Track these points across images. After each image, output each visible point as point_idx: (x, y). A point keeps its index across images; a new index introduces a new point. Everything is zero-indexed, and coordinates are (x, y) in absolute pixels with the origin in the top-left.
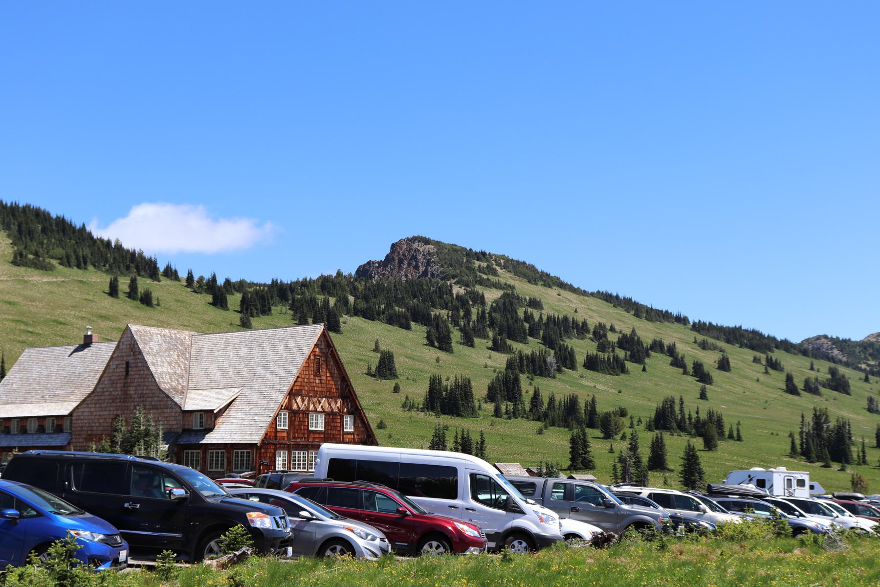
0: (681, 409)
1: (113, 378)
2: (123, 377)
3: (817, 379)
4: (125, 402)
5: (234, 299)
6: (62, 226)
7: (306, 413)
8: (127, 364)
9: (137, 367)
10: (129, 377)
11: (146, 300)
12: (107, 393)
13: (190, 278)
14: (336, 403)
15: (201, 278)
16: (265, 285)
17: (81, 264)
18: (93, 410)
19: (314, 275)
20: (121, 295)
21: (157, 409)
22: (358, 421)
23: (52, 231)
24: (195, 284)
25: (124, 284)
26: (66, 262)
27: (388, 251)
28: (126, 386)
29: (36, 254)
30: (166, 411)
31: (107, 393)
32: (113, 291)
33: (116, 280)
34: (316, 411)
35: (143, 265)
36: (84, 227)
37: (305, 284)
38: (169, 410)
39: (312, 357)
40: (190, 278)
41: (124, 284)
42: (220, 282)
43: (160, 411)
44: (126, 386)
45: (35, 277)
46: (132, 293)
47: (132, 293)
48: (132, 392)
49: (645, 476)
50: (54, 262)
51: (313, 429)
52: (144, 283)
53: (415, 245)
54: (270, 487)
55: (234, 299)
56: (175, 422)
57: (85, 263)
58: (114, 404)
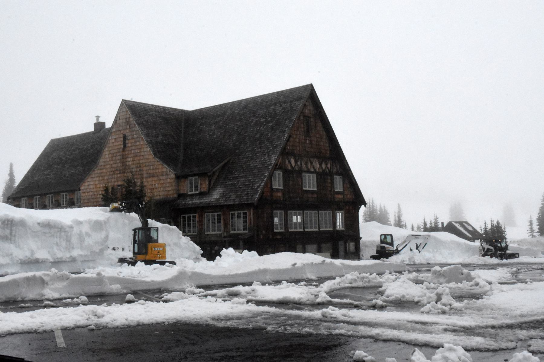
1: (112, 152)
2: (121, 150)
4: (124, 173)
7: (300, 172)
8: (125, 138)
9: (133, 138)
10: (128, 149)
12: (108, 166)
14: (327, 164)
18: (97, 183)
21: (153, 176)
22: (347, 181)
28: (124, 157)
30: (162, 178)
31: (108, 166)
34: (308, 171)
38: (164, 177)
39: (302, 118)
43: (156, 178)
44: (124, 157)
48: (130, 163)
49: (136, 262)
51: (307, 189)
54: (34, 277)
56: (170, 189)
58: (116, 176)
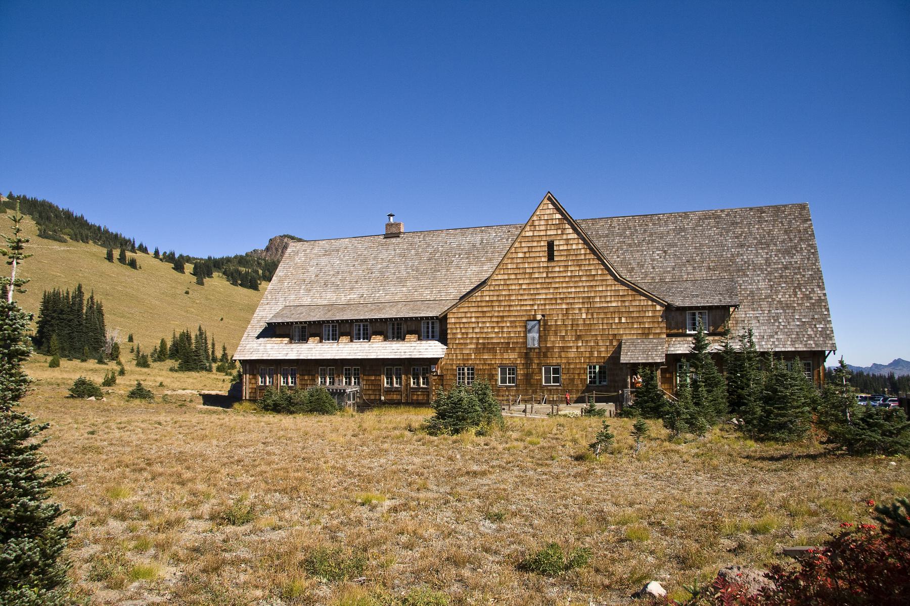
0: (213, 352)
3: (873, 453)
5: (189, 268)
6: (68, 215)
11: (133, 264)
13: (157, 253)
15: (165, 253)
16: (201, 259)
17: (85, 240)
19: (232, 255)
20: (115, 260)
23: (61, 218)
24: (161, 257)
25: (116, 253)
26: (75, 238)
27: (267, 244)
29: (55, 231)
32: (110, 257)
33: (111, 251)
35: (125, 244)
36: (82, 217)
37: (228, 260)
40: (157, 253)
41: (116, 253)
42: (177, 256)
45: (56, 246)
46: (122, 259)
47: (122, 259)
50: (66, 237)
52: (129, 255)
53: (286, 240)
55: (189, 268)
57: (87, 238)
